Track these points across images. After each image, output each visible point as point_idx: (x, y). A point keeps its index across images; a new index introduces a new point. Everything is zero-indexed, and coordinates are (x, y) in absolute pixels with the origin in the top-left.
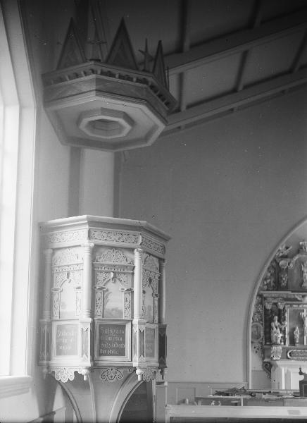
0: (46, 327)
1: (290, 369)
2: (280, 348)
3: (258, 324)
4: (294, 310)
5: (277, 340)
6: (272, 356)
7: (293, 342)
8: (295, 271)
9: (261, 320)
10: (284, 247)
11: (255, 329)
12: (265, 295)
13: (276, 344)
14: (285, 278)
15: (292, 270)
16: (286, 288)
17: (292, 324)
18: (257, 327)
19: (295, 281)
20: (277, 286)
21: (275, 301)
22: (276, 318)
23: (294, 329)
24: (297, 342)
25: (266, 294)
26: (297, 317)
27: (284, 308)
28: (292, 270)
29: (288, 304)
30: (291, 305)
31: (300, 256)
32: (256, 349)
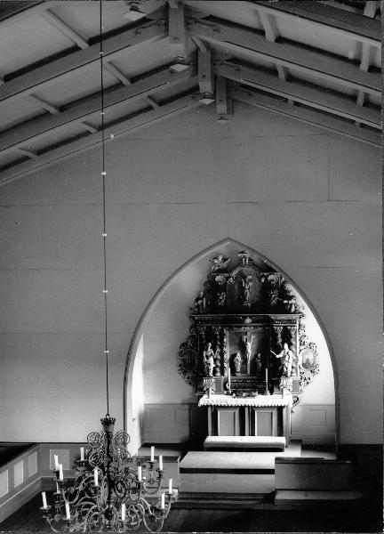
23: (235, 355)
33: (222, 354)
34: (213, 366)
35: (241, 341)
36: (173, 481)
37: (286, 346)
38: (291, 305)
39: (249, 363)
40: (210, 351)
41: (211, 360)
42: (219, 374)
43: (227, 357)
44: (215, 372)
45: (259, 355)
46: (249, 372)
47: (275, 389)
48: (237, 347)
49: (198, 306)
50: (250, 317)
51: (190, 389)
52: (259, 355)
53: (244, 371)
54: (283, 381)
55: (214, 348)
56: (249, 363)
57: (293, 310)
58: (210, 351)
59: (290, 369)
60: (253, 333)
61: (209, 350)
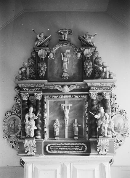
0: (95, 136)
1: (38, 167)
2: (34, 141)
3: (16, 117)
4: (55, 102)
5: (30, 132)
6: (26, 151)
7: (52, 134)
8: (56, 62)
9: (20, 113)
10: (42, 36)
11: (12, 122)
12: (89, 84)
13: (29, 138)
14: (43, 68)
15: (52, 61)
16: (45, 78)
17: (52, 116)
18: (14, 120)
19: (56, 72)
20: (36, 76)
21: (32, 91)
22: (32, 109)
23: (54, 121)
24: (57, 134)
25: (21, 84)
26: (58, 108)
27: (43, 98)
28: (52, 61)
29: (47, 95)
30: (51, 96)
31: (61, 46)
32: (12, 144)
33: (42, 118)
34: (34, 128)
35: (60, 108)
36: (51, 37)
37: (102, 109)
38: (106, 73)
39: (67, 128)
40: (31, 115)
41: (33, 122)
42: (39, 137)
43: (47, 122)
44: (36, 135)
45: (76, 121)
46: (66, 137)
47: (92, 151)
48: (56, 114)
49: (22, 74)
50: (69, 86)
51: (13, 152)
52: (76, 121)
53: (62, 135)
54: (101, 141)
55: (35, 112)
56: (67, 128)
57: (108, 76)
58: (31, 115)
59: (106, 131)
60: (70, 102)
61: (31, 113)
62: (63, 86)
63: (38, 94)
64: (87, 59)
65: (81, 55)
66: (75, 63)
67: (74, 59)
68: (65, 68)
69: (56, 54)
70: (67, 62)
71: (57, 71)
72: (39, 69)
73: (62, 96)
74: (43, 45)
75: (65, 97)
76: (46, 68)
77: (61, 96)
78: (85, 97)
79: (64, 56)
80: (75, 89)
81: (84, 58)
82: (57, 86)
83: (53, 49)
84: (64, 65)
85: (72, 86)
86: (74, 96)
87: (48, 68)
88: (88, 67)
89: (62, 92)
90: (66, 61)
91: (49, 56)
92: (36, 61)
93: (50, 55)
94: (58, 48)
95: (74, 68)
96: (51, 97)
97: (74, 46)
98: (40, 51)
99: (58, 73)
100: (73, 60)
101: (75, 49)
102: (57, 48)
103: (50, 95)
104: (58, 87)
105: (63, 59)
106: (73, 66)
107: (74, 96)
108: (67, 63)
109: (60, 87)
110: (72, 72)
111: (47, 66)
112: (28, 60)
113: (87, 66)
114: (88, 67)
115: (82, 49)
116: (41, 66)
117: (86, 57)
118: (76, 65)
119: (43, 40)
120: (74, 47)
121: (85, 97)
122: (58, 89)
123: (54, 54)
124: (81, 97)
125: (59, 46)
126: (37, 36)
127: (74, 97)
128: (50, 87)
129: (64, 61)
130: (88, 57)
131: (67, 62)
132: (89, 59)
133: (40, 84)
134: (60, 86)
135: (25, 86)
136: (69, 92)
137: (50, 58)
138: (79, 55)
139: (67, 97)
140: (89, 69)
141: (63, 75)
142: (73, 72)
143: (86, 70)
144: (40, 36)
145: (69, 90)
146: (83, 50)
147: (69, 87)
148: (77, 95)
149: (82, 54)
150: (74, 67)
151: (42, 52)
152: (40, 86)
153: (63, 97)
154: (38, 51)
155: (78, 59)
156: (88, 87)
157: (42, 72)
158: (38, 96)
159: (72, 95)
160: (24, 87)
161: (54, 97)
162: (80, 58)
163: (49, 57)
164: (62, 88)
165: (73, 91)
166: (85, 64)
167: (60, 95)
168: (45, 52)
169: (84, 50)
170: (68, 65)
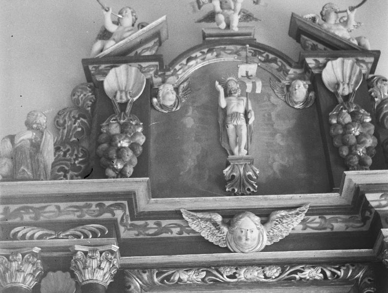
8: (190, 122)
10: (127, 21)
19: (190, 162)
28: (172, 119)
46: (339, 188)
50: (265, 215)
62: (230, 217)
63: (94, 251)
64: (340, 99)
65: (309, 90)
66: (284, 125)
67: (279, 109)
68: (238, 143)
69: (188, 89)
70: (246, 113)
71: (194, 157)
72: (105, 145)
73: (228, 271)
74: (133, 54)
75: (243, 275)
76: (141, 140)
77: (221, 269)
78: (360, 274)
79: (228, 94)
80: (298, 235)
81: (324, 101)
82: (200, 215)
83: (176, 71)
84: (231, 127)
85: (283, 213)
86: (299, 268)
87: (152, 141)
88: (356, 131)
89: (226, 250)
90: (241, 110)
91: (156, 96)
92: (91, 122)
93: (161, 94)
94: (200, 66)
95: (282, 144)
96: (168, 278)
97: (271, 56)
98: (112, 72)
99: (200, 166)
100: (273, 114)
101: (279, 70)
102: (195, 66)
103: (161, 268)
104: (207, 220)
105: (223, 103)
106: (273, 135)
107: (299, 268)
108: (247, 120)
109: (215, 224)
110: (274, 161)
111: (146, 132)
112: (59, 114)
113: (346, 127)
114: (356, 131)
115: (310, 62)
116: (115, 129)
117: (334, 95)
118: (289, 131)
119: (130, 33)
120: (274, 61)
121: (360, 274)
122: (204, 234)
123: (180, 90)
124: (333, 274)
125: (203, 59)
126: (104, 18)
127: (296, 272)
128: (165, 223)
129: (229, 112)
130: (346, 93)
131: (246, 113)
132: (352, 99)
133: (107, 203)
134: (218, 218)
135: (27, 218)
136: (267, 249)
137: (162, 106)
138: (301, 90)
139: (255, 274)
140: (357, 137)
141: (227, 171)
142: (278, 162)
143: (345, 143)
144: (117, 23)
145: (266, 242)
146: (315, 68)
147: (263, 223)
148: (313, 263)
149: (315, 81)
150: (279, 140)
151: (123, 79)
152: (107, 216)
153: (233, 276)
154: (105, 74)
155: (297, 106)
156: (364, 219)
157: (120, 157)
158: (94, 263)
159: (283, 264)
160: (18, 220)
161: (185, 276)
162: (306, 101)
163: (155, 100)
164: (225, 229)
165: (291, 246)
166: (334, 121)
167: (218, 266)
168: (137, 77)
169: (325, 65)
170: (249, 128)
